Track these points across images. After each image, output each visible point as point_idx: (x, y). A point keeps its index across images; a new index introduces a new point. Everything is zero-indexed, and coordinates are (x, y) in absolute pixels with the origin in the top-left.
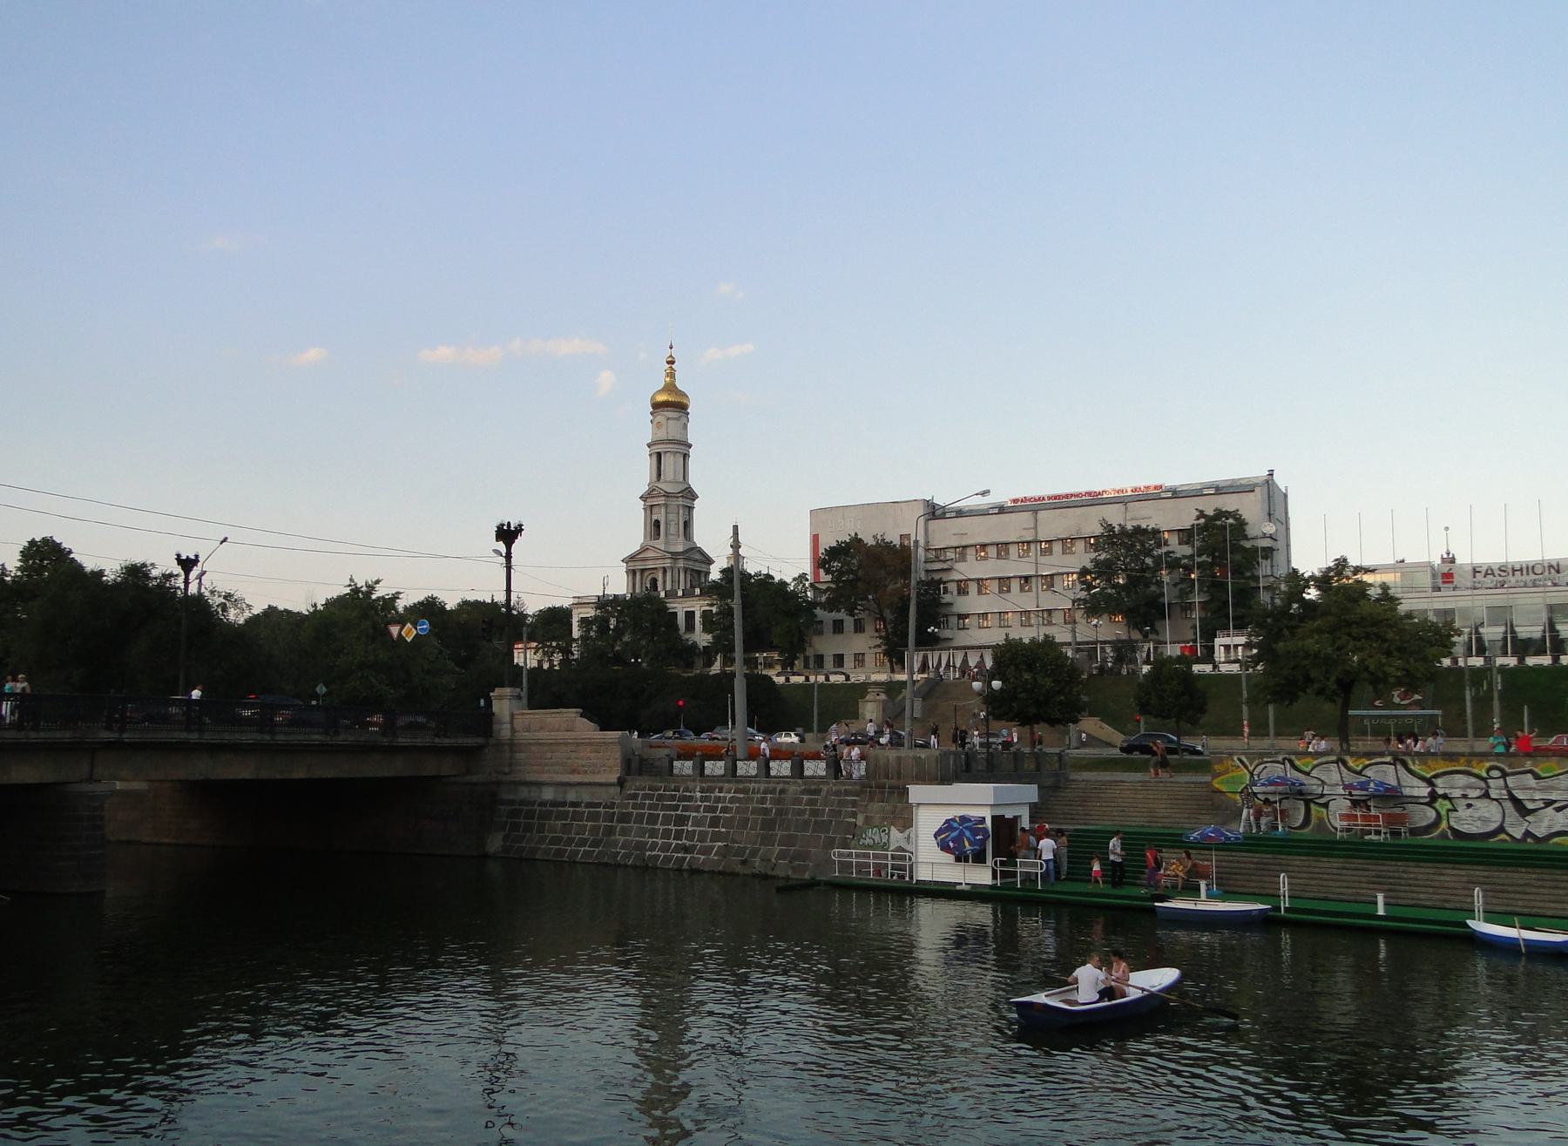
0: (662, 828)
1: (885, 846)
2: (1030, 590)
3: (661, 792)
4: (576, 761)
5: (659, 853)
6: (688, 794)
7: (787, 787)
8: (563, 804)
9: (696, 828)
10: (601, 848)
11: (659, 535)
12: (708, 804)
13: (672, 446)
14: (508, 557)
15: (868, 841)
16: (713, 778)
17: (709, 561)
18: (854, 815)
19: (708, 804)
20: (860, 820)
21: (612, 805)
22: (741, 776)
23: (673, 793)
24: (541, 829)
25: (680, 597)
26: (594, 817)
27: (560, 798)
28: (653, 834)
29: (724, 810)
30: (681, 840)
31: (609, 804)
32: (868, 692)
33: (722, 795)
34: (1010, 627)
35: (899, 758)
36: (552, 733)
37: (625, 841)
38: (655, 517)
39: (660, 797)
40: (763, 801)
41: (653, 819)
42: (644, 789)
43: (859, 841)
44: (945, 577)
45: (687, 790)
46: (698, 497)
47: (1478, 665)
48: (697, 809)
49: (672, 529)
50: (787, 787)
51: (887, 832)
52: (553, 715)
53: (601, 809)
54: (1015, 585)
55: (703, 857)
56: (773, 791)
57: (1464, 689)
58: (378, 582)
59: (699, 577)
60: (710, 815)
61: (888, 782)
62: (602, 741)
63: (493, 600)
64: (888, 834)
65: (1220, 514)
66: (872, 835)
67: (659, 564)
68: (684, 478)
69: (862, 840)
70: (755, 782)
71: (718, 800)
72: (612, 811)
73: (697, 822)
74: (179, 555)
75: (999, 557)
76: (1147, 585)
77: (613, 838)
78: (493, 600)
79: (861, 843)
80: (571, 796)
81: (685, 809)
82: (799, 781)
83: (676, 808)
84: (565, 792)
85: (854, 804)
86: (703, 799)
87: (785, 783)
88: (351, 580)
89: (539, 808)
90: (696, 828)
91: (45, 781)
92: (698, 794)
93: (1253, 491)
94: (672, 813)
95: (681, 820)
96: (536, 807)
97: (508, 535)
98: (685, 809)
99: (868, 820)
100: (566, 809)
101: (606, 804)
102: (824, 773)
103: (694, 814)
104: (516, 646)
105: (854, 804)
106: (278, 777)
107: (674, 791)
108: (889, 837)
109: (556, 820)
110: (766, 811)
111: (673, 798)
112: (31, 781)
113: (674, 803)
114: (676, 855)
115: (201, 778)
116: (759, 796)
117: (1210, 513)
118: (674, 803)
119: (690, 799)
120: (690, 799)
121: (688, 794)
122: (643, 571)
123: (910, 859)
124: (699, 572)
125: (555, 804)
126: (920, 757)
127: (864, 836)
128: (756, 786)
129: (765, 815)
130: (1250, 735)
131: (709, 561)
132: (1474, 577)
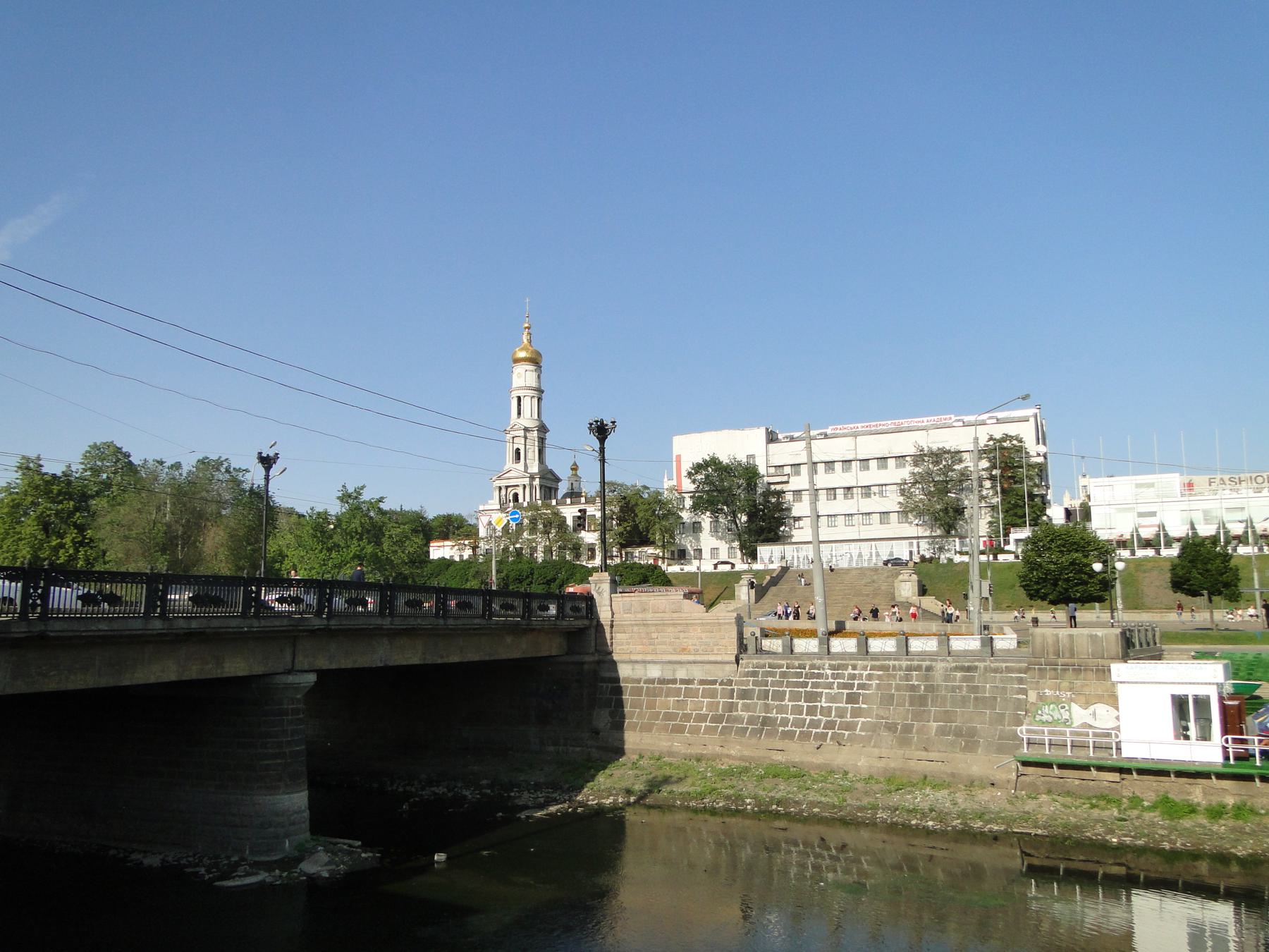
0: (790, 704)
1: (1066, 723)
2: (852, 498)
3: (784, 669)
4: (685, 640)
5: (794, 729)
6: (816, 671)
7: (934, 664)
8: (674, 681)
9: (831, 705)
10: (724, 724)
11: (519, 459)
12: (842, 681)
13: (528, 391)
14: (602, 450)
15: (1045, 718)
16: (843, 656)
17: (558, 480)
18: (1024, 692)
19: (842, 681)
20: (1032, 696)
21: (730, 682)
22: (875, 654)
23: (798, 670)
24: (651, 706)
25: (584, 504)
26: (713, 694)
27: (669, 676)
28: (782, 709)
29: (861, 686)
30: (816, 716)
31: (725, 681)
32: (742, 578)
33: (856, 672)
34: (802, 528)
35: (1071, 636)
36: (657, 615)
37: (827, 722)
38: (516, 446)
39: (784, 675)
40: (907, 678)
41: (779, 696)
42: (764, 666)
43: (1035, 717)
44: (785, 487)
45: (812, 667)
46: (549, 431)
47: (1151, 556)
48: (830, 686)
49: (530, 455)
50: (934, 664)
51: (1067, 708)
52: (657, 598)
53: (717, 686)
54: (840, 492)
55: (847, 733)
56: (918, 668)
57: (1253, 572)
58: (363, 487)
59: (550, 492)
60: (846, 691)
61: (1060, 661)
62: (716, 621)
63: (401, 509)
64: (1069, 710)
65: (1006, 437)
66: (1048, 712)
67: (520, 482)
68: (538, 417)
69: (1037, 716)
70: (895, 660)
71: (853, 677)
72: (729, 688)
73: (832, 699)
74: (260, 453)
75: (897, 467)
76: (230, 546)
77: (735, 713)
78: (401, 509)
79: (1037, 719)
80: (681, 674)
81: (815, 685)
82: (948, 658)
83: (805, 685)
84: (674, 671)
85: (1021, 681)
86: (835, 676)
87: (932, 660)
88: (344, 486)
89: (645, 685)
90: (831, 705)
91: (254, 673)
92: (829, 672)
93: (1028, 421)
94: (801, 690)
95: (812, 697)
96: (642, 684)
97: (601, 431)
98: (815, 685)
99: (1041, 698)
100: (678, 686)
101: (722, 681)
102: (816, 650)
103: (827, 691)
104: (431, 545)
105: (1021, 681)
106: (440, 661)
107: (799, 667)
108: (1070, 713)
109: (666, 696)
110: (913, 688)
111: (799, 675)
112: (241, 674)
113: (801, 680)
114: (814, 731)
115: (380, 665)
116: (902, 672)
117: (998, 436)
118: (801, 680)
119: (819, 676)
120: (819, 676)
121: (816, 671)
122: (507, 487)
123: (1117, 736)
124: (550, 489)
125: (662, 681)
126: (1096, 635)
127: (1040, 712)
128: (896, 663)
129: (911, 691)
130: (1123, 609)
131: (558, 480)
132: (1210, 485)
